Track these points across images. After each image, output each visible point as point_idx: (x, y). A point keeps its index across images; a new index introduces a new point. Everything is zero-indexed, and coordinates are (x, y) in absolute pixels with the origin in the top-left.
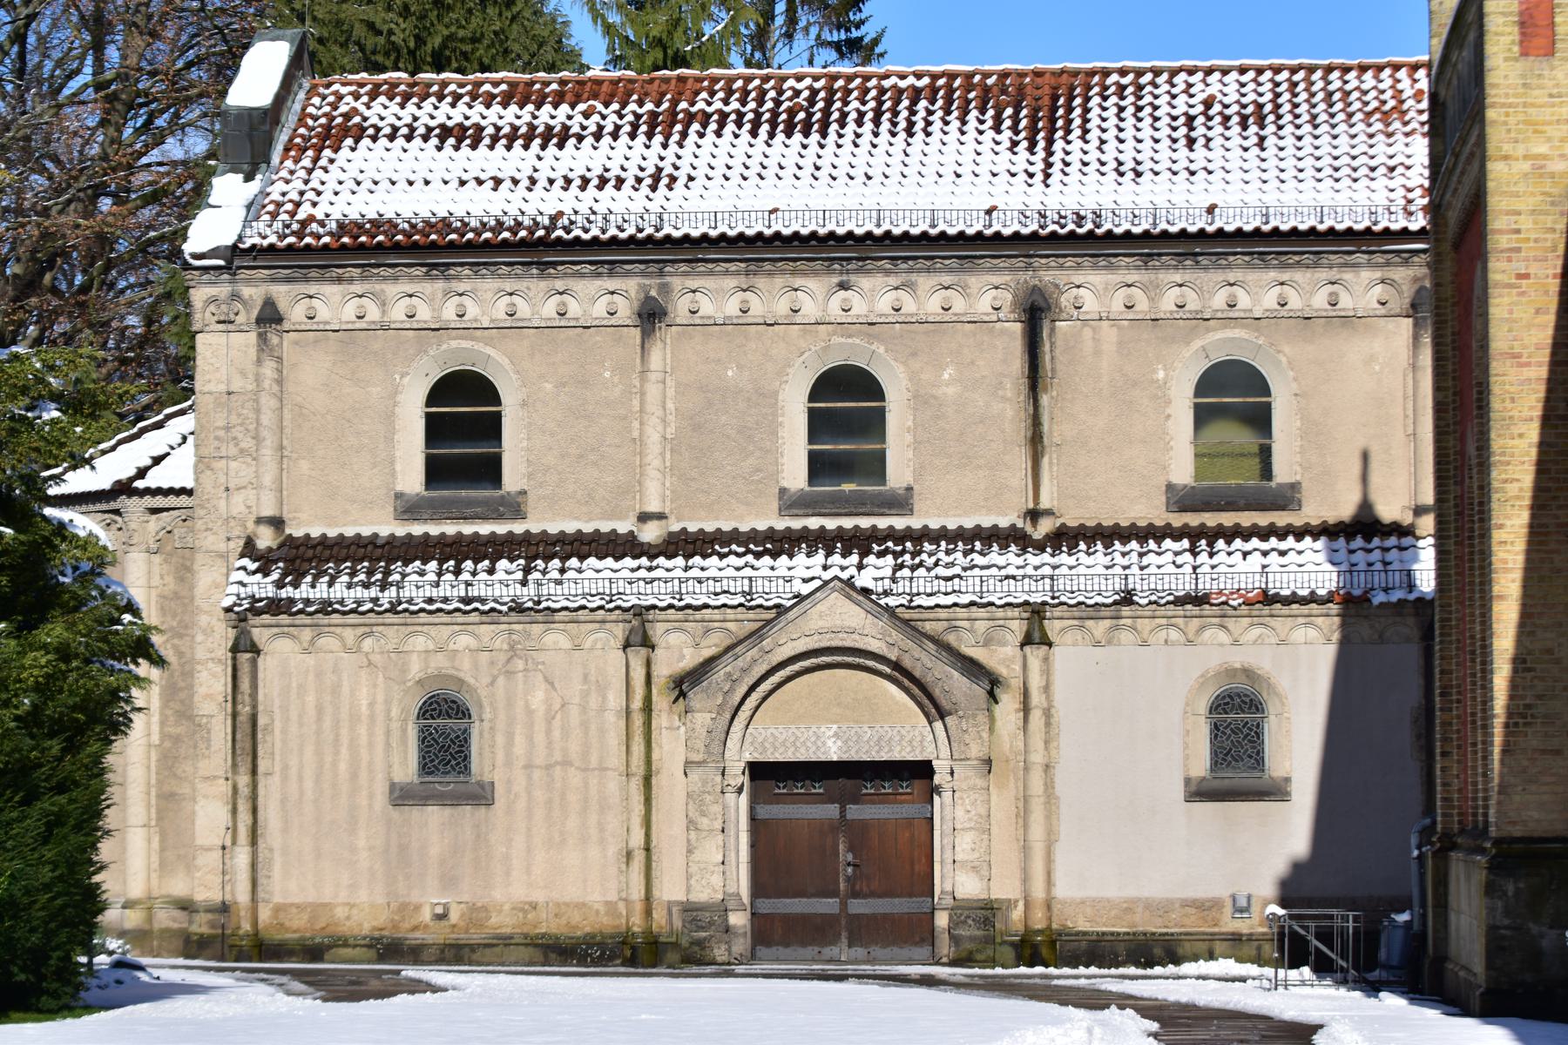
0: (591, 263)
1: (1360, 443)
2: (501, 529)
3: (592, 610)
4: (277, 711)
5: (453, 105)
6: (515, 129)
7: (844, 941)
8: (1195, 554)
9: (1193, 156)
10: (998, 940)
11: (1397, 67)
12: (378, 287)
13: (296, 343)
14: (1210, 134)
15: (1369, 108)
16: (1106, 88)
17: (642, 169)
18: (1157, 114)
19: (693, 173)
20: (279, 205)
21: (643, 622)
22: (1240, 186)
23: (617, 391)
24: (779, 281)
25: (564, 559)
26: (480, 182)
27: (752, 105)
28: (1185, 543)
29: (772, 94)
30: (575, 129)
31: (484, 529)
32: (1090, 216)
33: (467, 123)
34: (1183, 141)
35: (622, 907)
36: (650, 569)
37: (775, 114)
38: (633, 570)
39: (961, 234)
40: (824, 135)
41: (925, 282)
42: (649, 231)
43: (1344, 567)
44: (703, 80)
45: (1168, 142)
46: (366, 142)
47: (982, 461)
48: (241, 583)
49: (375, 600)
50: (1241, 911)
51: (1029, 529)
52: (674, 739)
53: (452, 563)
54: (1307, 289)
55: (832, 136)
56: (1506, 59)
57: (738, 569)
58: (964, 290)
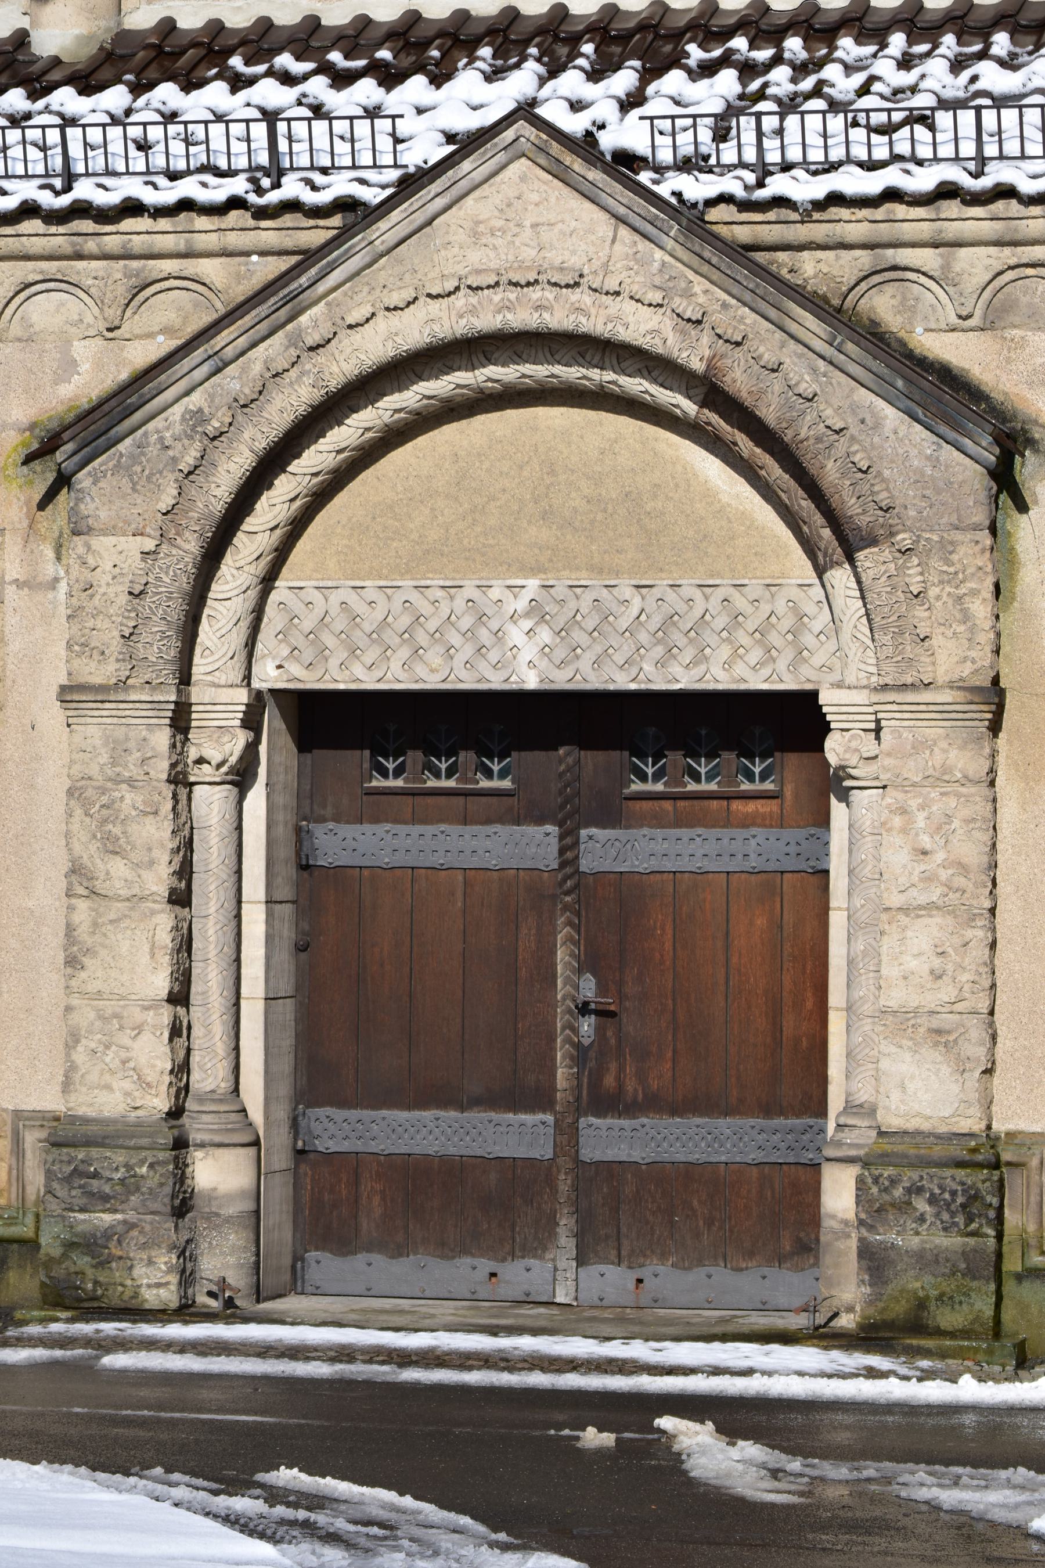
7: (566, 1242)
10: (1012, 1264)
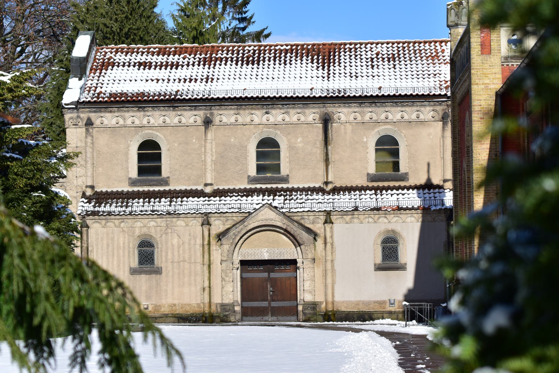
0: (189, 106)
1: (427, 160)
2: (162, 189)
3: (192, 214)
4: (94, 245)
5: (142, 55)
6: (162, 63)
7: (270, 315)
8: (376, 195)
9: (373, 71)
11: (436, 42)
12: (123, 114)
13: (98, 131)
14: (378, 64)
15: (427, 55)
16: (346, 49)
17: (203, 76)
18: (362, 57)
19: (219, 77)
20: (90, 88)
21: (208, 217)
22: (388, 81)
23: (197, 146)
24: (247, 111)
25: (182, 198)
26: (152, 80)
27: (235, 55)
28: (373, 192)
29: (241, 51)
30: (181, 63)
31: (157, 189)
32: (343, 90)
33: (147, 61)
34: (370, 66)
35: (202, 305)
36: (209, 201)
37: (243, 58)
38: (203, 201)
39: (303, 97)
40: (259, 65)
41: (292, 111)
42: (206, 96)
43: (422, 199)
44: (219, 47)
45: (366, 67)
46: (115, 67)
47: (310, 167)
48: (83, 206)
49: (124, 211)
50: (392, 304)
51: (325, 187)
52: (217, 254)
53: (147, 199)
54: (410, 113)
55: (261, 65)
56: (477, 56)
57: (236, 201)
58: (304, 114)
